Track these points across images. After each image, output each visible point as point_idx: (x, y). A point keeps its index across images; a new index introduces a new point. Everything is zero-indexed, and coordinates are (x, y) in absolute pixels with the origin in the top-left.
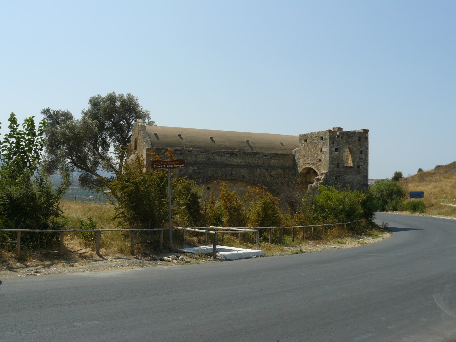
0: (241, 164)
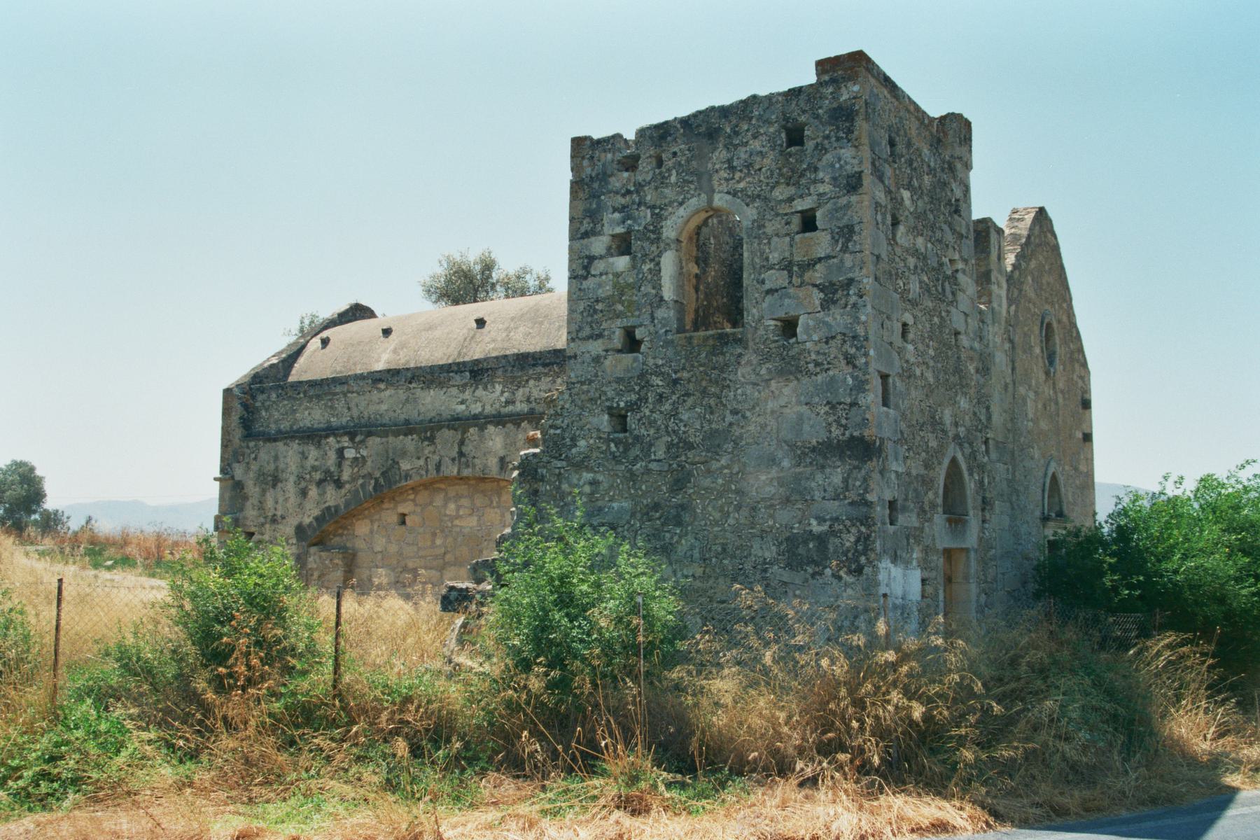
0: (510, 408)
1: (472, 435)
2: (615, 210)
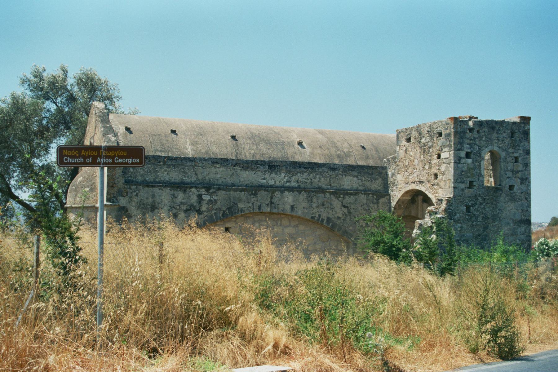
0: (288, 184)
1: (277, 195)
2: (468, 144)
